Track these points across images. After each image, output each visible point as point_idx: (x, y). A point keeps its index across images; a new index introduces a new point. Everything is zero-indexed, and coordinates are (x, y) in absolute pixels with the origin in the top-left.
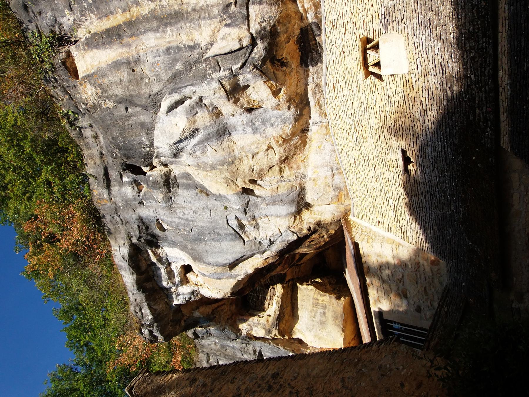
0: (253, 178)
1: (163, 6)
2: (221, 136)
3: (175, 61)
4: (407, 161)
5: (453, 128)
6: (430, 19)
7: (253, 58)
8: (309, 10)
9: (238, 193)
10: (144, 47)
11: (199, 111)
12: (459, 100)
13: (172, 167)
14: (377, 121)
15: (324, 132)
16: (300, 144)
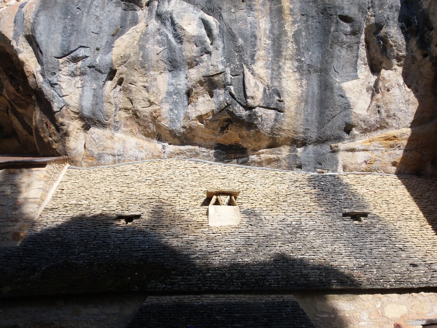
0: (124, 82)
1: (287, 43)
2: (170, 62)
3: (245, 40)
4: (129, 219)
5: (162, 258)
6: (252, 245)
7: (236, 105)
8: (258, 157)
9: (112, 64)
10: (260, 17)
11: (199, 48)
12: (187, 264)
13: (145, 10)
14: (166, 198)
15: (155, 154)
16: (148, 132)
